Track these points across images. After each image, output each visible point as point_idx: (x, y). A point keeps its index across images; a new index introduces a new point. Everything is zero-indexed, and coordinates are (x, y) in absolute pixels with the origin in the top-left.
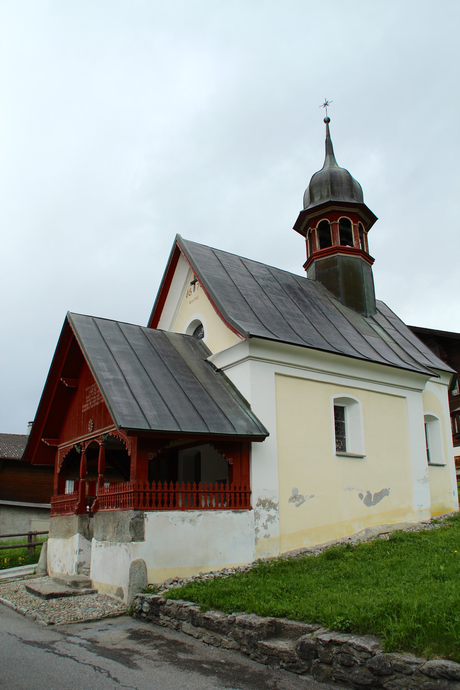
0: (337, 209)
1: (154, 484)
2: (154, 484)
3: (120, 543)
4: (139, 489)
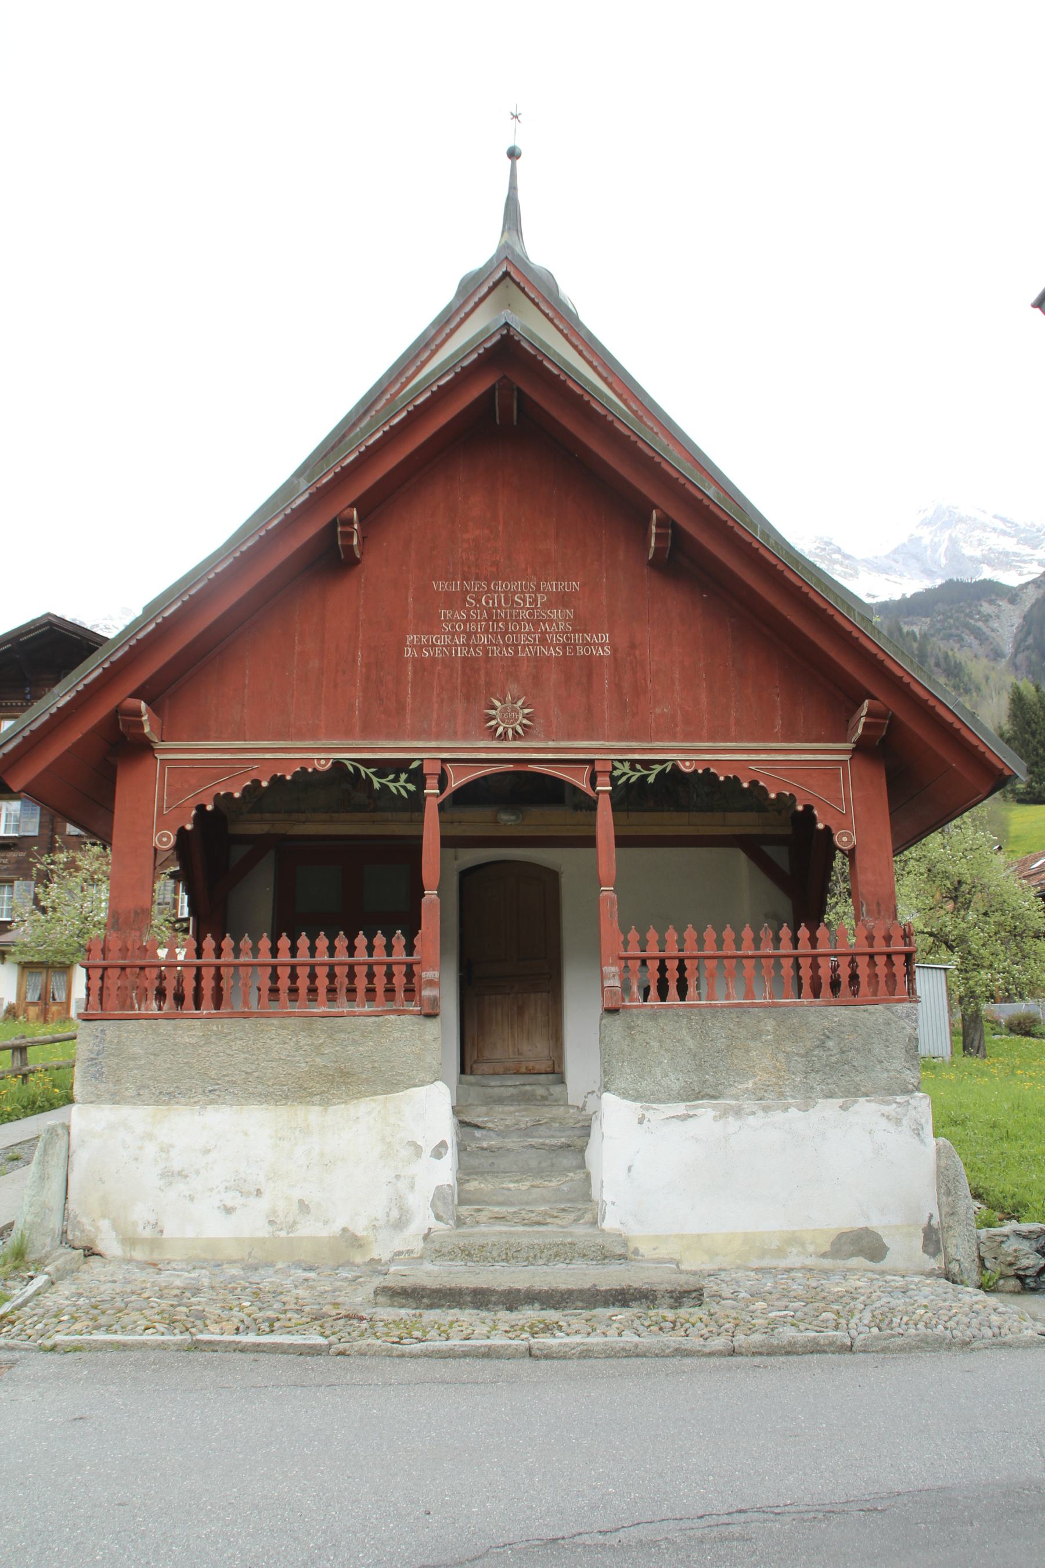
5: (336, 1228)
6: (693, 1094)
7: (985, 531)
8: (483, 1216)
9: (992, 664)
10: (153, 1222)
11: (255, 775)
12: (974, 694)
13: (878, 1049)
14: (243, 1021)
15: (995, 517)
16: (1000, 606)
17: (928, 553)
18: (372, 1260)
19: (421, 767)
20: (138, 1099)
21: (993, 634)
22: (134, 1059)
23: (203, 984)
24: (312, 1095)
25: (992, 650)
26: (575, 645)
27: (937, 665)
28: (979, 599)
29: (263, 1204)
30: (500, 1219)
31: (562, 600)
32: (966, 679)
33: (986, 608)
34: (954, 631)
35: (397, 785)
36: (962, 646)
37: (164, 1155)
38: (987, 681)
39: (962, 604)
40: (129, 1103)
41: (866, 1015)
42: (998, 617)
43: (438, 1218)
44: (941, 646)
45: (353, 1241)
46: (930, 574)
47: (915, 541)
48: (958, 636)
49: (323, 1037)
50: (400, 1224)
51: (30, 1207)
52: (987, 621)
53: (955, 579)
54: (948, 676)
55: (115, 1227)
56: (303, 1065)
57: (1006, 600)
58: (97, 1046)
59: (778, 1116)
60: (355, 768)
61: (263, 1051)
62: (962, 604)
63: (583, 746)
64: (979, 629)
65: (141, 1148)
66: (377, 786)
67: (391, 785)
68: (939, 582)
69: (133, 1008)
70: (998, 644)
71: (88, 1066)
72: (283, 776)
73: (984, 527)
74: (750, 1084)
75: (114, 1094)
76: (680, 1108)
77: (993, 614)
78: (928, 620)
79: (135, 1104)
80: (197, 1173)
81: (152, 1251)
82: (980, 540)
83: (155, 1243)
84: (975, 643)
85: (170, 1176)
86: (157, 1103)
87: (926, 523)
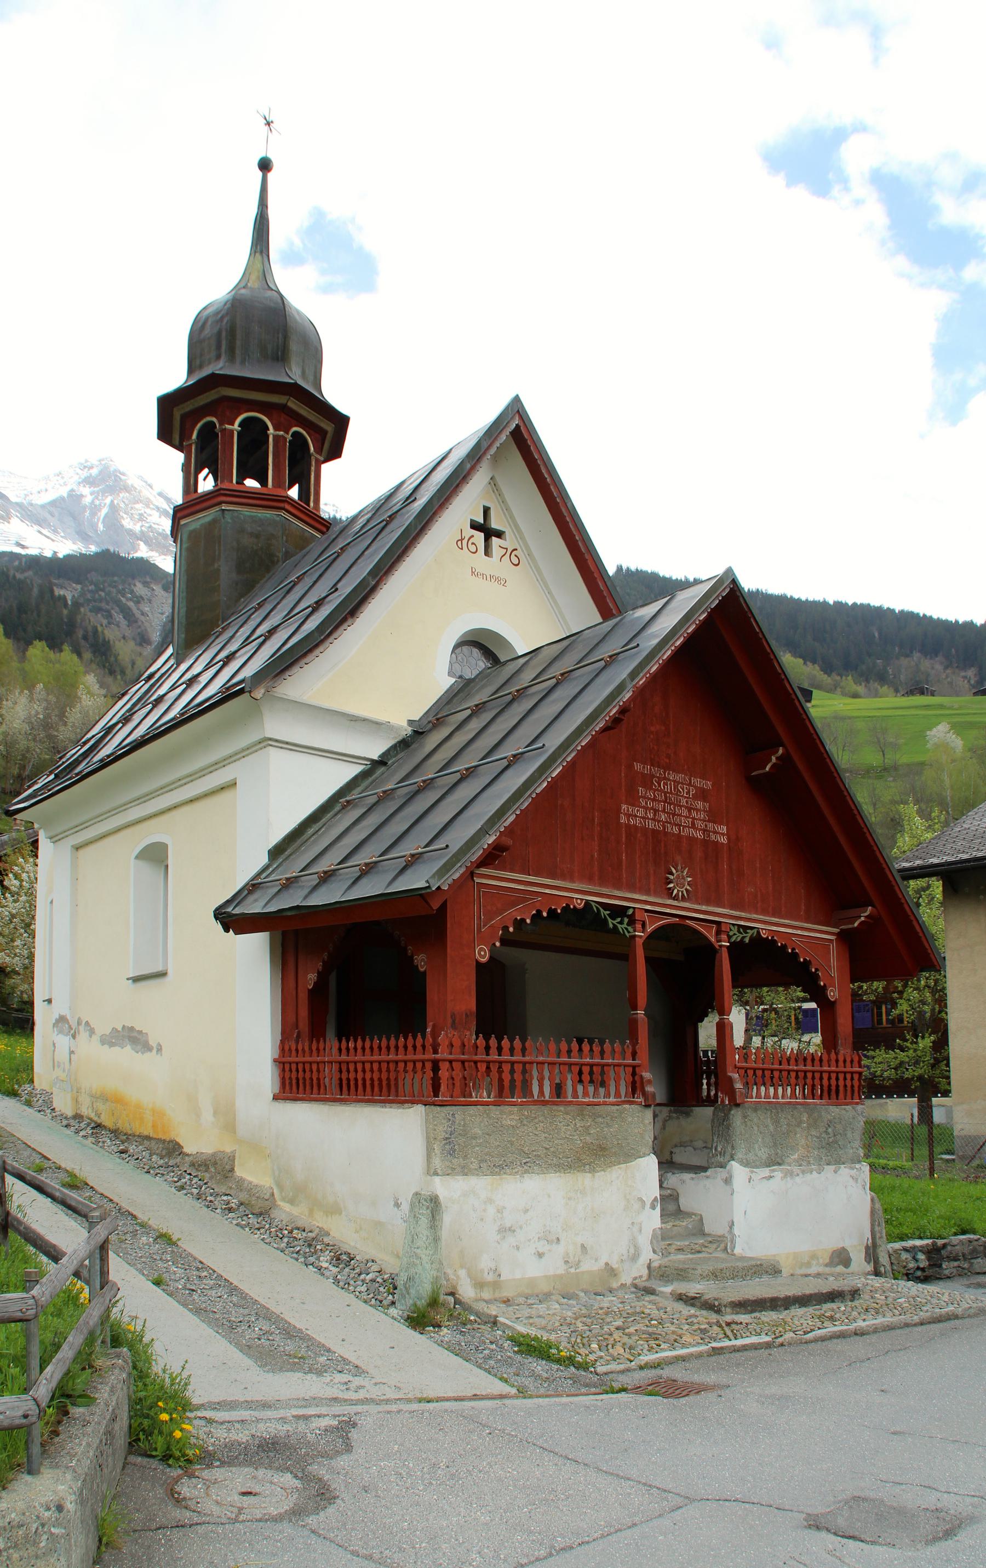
0: (202, 403)
1: (493, 1042)
2: (493, 1042)
3: (833, 1167)
4: (406, 1055)
5: (601, 1264)
6: (774, 1162)
7: (148, 506)
8: (672, 1249)
9: (139, 649)
10: (494, 1268)
11: (538, 906)
12: (119, 677)
13: (849, 1134)
14: (543, 1107)
15: (160, 494)
16: (153, 590)
17: (87, 514)
18: (622, 1284)
19: (634, 912)
20: (479, 1172)
21: (142, 618)
22: (475, 1138)
23: (503, 1075)
24: (584, 1165)
25: (139, 634)
26: (709, 831)
27: (85, 638)
28: (133, 578)
29: (560, 1249)
30: (680, 1250)
31: (702, 794)
32: (112, 659)
33: (140, 589)
34: (103, 605)
35: (623, 926)
36: (109, 623)
37: (499, 1215)
38: (133, 667)
39: (116, 578)
40: (473, 1175)
41: (844, 1112)
42: (150, 601)
43: (654, 1252)
44: (92, 620)
45: (611, 1271)
46: (84, 537)
47: (74, 497)
48: (108, 611)
49: (590, 1120)
50: (634, 1258)
51: (431, 1264)
52: (138, 602)
53: (112, 550)
54: (94, 652)
55: (469, 1275)
56: (579, 1142)
57: (160, 586)
58: (450, 1127)
59: (808, 1177)
60: (597, 908)
61: (556, 1131)
62: (116, 578)
63: (721, 913)
64: (129, 609)
65: (485, 1210)
66: (611, 926)
67: (619, 926)
68: (93, 549)
69: (471, 1096)
70: (146, 630)
71: (445, 1145)
72: (556, 909)
73: (148, 503)
74: (796, 1156)
75: (463, 1167)
76: (766, 1172)
77: (145, 597)
78: (79, 587)
79: (477, 1175)
80: (521, 1228)
81: (494, 1291)
82: (141, 515)
83: (496, 1285)
84: (124, 623)
85: (506, 1231)
86: (492, 1174)
87: (89, 481)
